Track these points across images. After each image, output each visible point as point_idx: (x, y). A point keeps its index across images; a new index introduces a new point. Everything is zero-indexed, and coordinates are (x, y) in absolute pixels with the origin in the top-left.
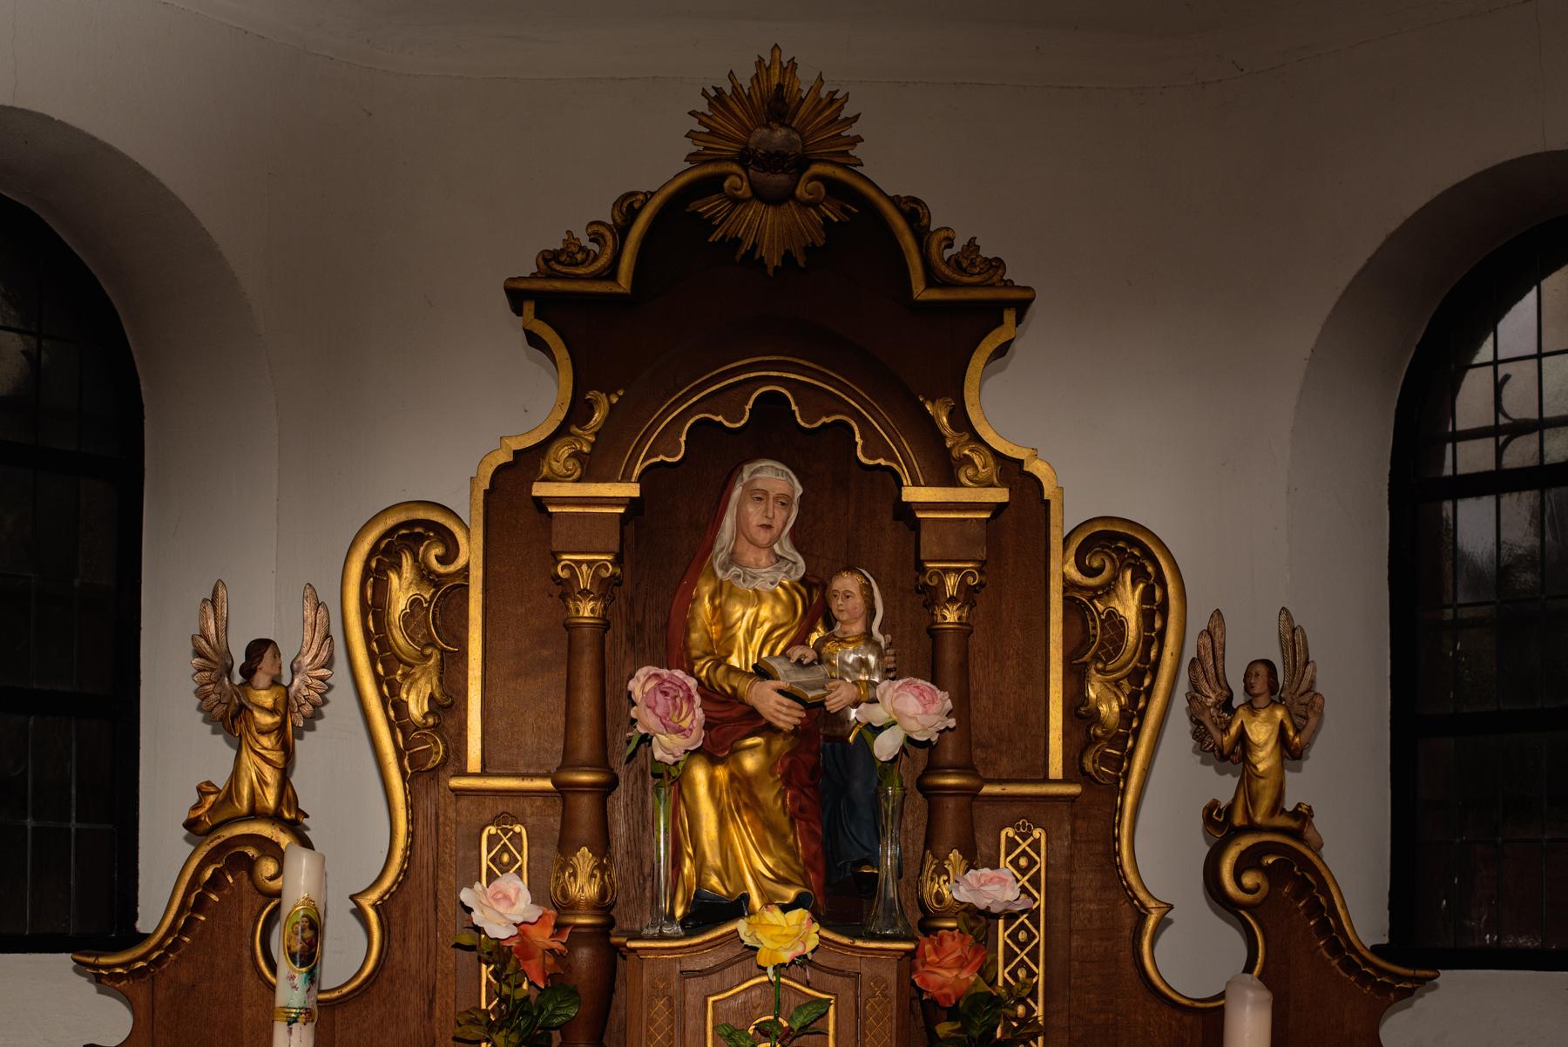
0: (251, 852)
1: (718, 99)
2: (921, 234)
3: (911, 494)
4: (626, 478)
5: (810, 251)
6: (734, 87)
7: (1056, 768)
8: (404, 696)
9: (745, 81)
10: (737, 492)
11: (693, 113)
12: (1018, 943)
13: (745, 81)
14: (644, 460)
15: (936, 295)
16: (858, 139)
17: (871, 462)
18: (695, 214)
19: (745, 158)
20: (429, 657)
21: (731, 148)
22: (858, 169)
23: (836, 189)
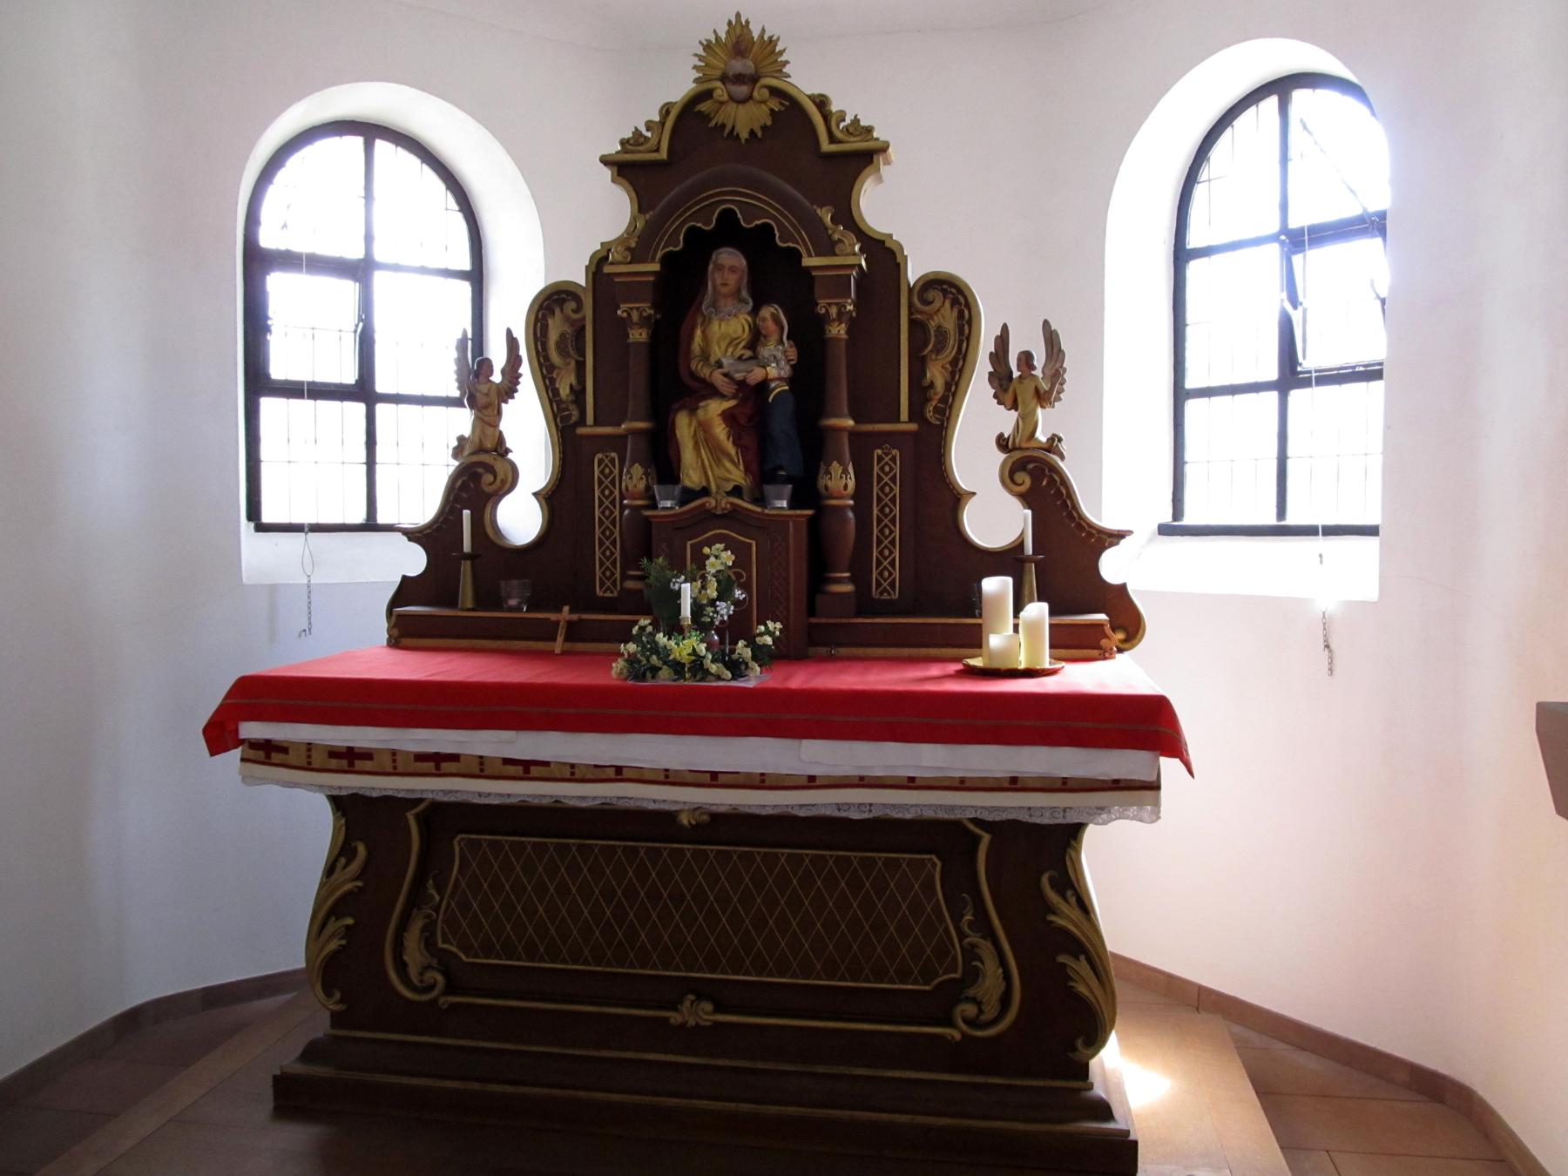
0: (480, 470)
1: (708, 47)
2: (826, 116)
3: (807, 261)
4: (653, 260)
5: (764, 128)
6: (716, 39)
7: (904, 415)
8: (557, 386)
9: (723, 36)
10: (711, 267)
11: (696, 55)
12: (605, 536)
13: (723, 36)
14: (663, 249)
15: (834, 148)
16: (787, 62)
17: (682, 244)
18: (699, 112)
19: (724, 79)
20: (569, 364)
21: (718, 73)
22: (788, 80)
23: (776, 92)
